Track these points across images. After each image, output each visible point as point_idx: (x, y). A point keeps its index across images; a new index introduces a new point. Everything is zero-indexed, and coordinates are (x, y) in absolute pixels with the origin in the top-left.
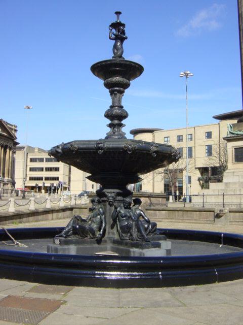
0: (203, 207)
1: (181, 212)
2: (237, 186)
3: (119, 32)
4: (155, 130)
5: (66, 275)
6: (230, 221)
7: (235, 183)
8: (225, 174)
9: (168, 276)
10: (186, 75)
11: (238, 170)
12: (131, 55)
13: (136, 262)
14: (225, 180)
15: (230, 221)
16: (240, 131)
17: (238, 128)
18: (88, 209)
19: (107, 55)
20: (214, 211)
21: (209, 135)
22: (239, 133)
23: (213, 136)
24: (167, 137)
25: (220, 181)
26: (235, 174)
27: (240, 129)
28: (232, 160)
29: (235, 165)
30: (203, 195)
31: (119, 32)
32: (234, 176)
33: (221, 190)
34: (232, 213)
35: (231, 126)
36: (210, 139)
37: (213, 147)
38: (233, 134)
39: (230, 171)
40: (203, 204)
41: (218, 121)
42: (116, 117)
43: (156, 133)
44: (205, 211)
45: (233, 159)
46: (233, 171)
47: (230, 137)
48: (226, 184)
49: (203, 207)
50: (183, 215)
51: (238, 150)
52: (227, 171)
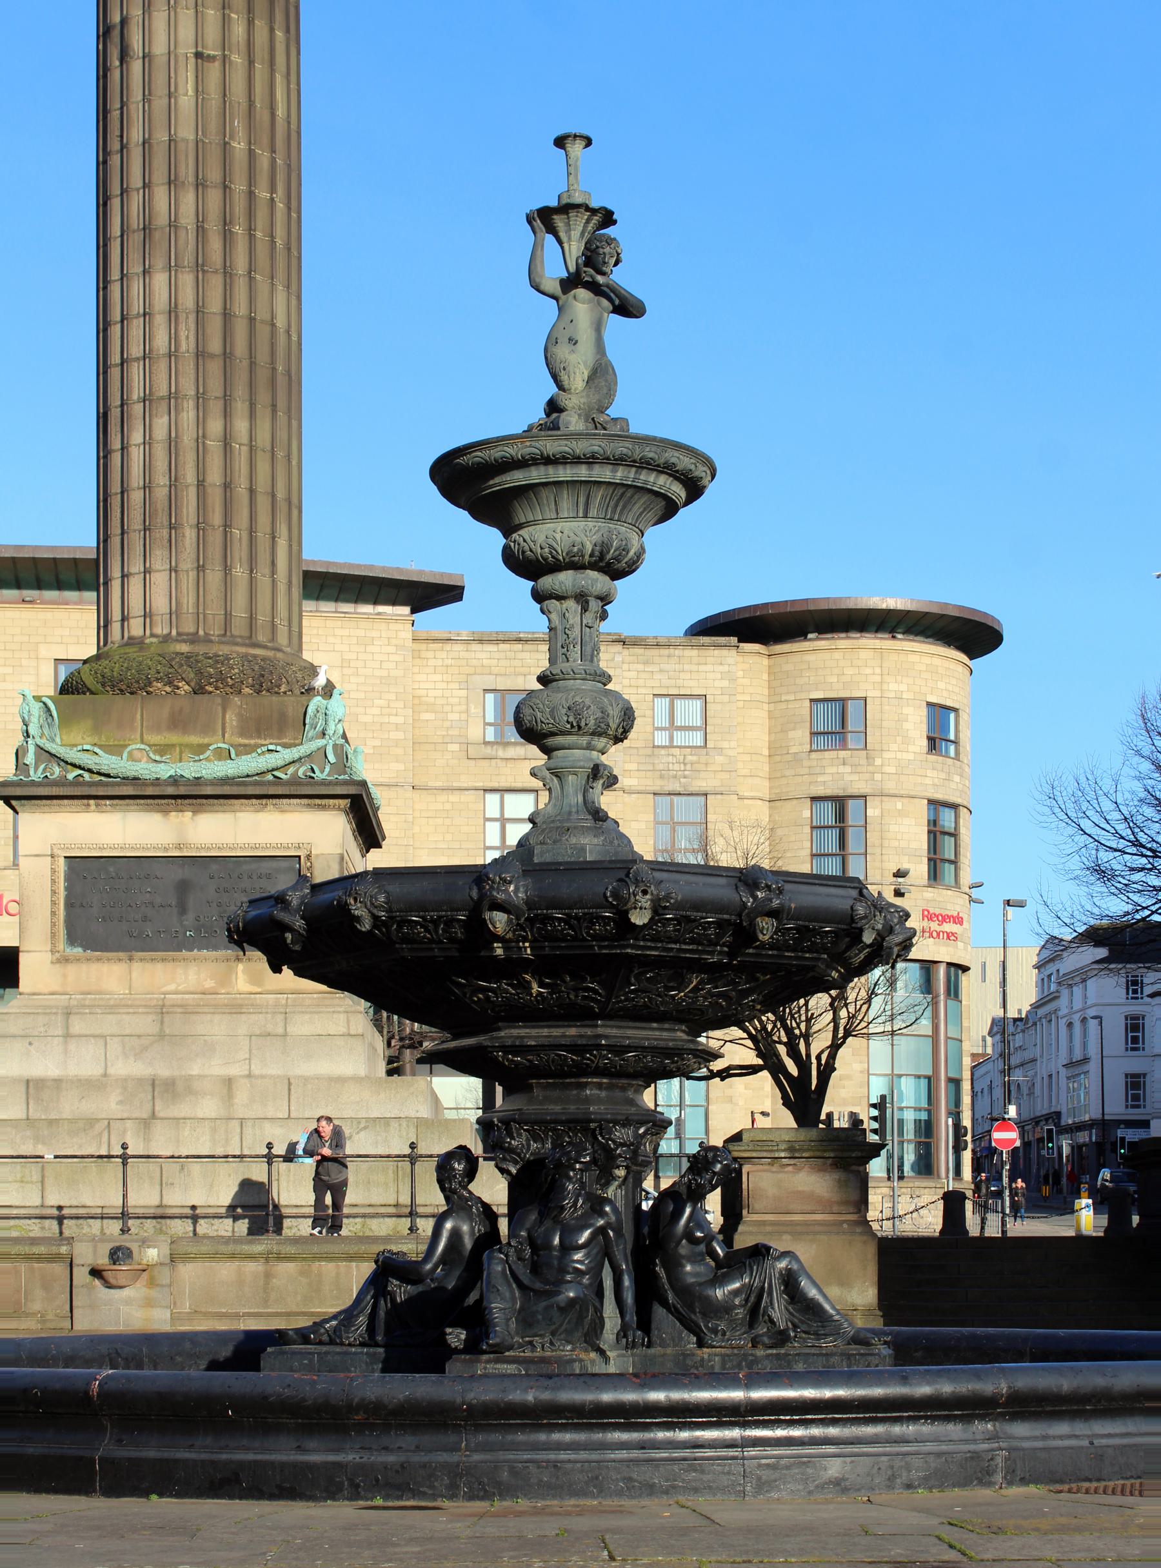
12: (651, 404)
16: (115, 750)
17: (97, 729)
29: (71, 969)
32: (67, 1036)
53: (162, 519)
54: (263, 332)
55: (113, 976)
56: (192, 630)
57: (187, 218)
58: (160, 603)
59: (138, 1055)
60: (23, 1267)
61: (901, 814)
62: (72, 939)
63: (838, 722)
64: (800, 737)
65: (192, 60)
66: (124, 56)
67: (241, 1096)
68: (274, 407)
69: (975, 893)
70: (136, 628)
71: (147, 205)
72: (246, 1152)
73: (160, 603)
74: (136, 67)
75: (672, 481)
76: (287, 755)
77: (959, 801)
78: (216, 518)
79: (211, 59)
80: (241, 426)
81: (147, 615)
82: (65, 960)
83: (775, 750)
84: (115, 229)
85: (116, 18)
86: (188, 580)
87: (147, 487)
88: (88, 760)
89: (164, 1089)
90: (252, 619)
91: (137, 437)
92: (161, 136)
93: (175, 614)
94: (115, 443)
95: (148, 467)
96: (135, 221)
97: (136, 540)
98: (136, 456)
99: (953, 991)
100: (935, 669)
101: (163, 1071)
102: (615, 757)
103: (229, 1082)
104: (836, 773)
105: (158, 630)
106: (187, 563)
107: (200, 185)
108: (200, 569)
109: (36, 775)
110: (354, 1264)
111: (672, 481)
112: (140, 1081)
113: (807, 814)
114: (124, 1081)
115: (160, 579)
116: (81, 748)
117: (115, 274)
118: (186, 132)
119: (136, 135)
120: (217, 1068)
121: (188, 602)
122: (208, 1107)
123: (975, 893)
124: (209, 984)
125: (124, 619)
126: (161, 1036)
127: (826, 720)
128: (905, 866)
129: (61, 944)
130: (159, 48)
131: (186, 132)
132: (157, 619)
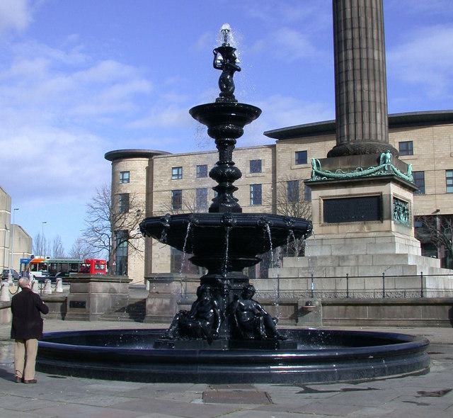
2: (329, 263)
3: (227, 61)
6: (324, 320)
7: (324, 258)
9: (342, 369)
11: (330, 237)
12: (242, 96)
13: (315, 355)
14: (308, 253)
15: (324, 320)
16: (334, 171)
17: (329, 167)
19: (211, 95)
24: (178, 168)
27: (334, 167)
28: (320, 220)
29: (324, 228)
31: (227, 61)
32: (322, 245)
33: (303, 269)
34: (326, 308)
35: (317, 162)
36: (260, 174)
37: (263, 187)
39: (317, 237)
44: (425, 305)
45: (320, 218)
46: (320, 237)
47: (317, 181)
48: (314, 258)
51: (329, 202)
54: (371, 62)
55: (333, 228)
59: (339, 249)
62: (325, 221)
67: (361, 260)
68: (375, 80)
75: (250, 113)
76: (375, 169)
80: (365, 86)
82: (322, 226)
89: (342, 258)
90: (370, 134)
101: (345, 253)
103: (357, 256)
111: (250, 113)
116: (326, 172)
120: (358, 252)
122: (353, 263)
124: (357, 230)
126: (345, 244)
129: (322, 222)
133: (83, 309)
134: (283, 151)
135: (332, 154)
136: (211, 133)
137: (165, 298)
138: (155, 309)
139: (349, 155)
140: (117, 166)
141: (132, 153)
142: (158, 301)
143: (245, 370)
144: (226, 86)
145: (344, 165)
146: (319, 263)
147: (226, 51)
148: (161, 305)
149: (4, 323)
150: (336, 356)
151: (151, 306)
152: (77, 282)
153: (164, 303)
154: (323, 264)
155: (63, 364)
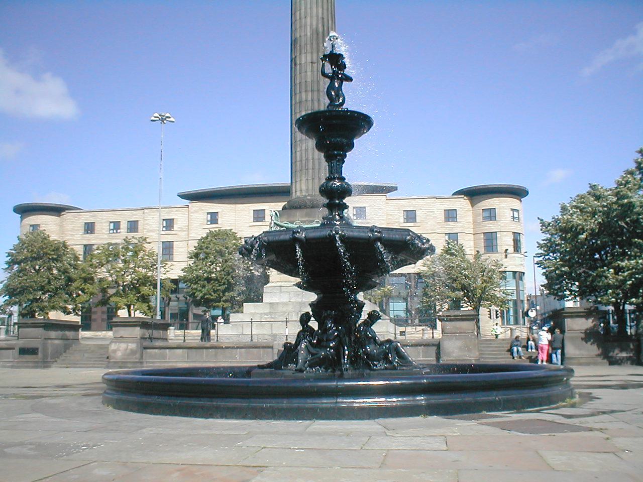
0: (252, 340)
1: (213, 350)
4: (68, 209)
5: (508, 412)
7: (285, 304)
8: (266, 288)
10: (163, 119)
12: (354, 99)
14: (267, 298)
18: (17, 349)
20: (271, 347)
21: (169, 224)
22: (290, 225)
23: (176, 227)
25: (259, 299)
26: (283, 289)
30: (252, 322)
32: (281, 292)
35: (276, 214)
38: (278, 225)
40: (252, 337)
41: (187, 202)
42: (335, 196)
43: (67, 215)
46: (279, 284)
48: (272, 305)
49: (252, 340)
50: (216, 355)
52: (269, 285)
53: (304, 168)
56: (311, 193)
57: (310, 98)
58: (304, 187)
60: (262, 350)
61: (506, 236)
63: (491, 215)
64: (480, 219)
65: (310, 64)
66: (295, 65)
69: (526, 254)
70: (298, 194)
71: (301, 97)
72: (394, 333)
73: (304, 187)
74: (298, 67)
77: (520, 232)
78: (317, 167)
79: (315, 63)
81: (301, 190)
83: (475, 222)
84: (294, 102)
85: (294, 57)
86: (310, 182)
87: (301, 161)
88: (286, 225)
91: (299, 149)
92: (303, 81)
93: (307, 190)
94: (294, 151)
95: (301, 156)
96: (298, 101)
97: (298, 173)
98: (298, 154)
99: (521, 279)
100: (512, 202)
102: (347, 201)
104: (490, 227)
105: (303, 194)
106: (310, 178)
107: (312, 91)
108: (313, 179)
109: (273, 229)
110: (435, 359)
112: (297, 303)
113: (483, 236)
114: (293, 303)
115: (303, 182)
117: (294, 113)
118: (309, 80)
119: (298, 82)
121: (310, 187)
123: (526, 254)
125: (296, 192)
127: (487, 214)
128: (507, 248)
130: (303, 62)
131: (309, 80)
132: (303, 191)
133: (34, 356)
134: (196, 212)
135: (284, 208)
136: (320, 147)
137: (130, 343)
138: (119, 354)
139: (307, 208)
140: (23, 222)
141: (32, 206)
142: (123, 346)
143: (369, 402)
144: (335, 94)
145: (302, 217)
146: (281, 309)
147: (335, 59)
148: (126, 349)
149: (183, 351)
150: (424, 384)
151: (115, 351)
152: (28, 327)
153: (129, 347)
154: (284, 309)
155: (186, 401)
